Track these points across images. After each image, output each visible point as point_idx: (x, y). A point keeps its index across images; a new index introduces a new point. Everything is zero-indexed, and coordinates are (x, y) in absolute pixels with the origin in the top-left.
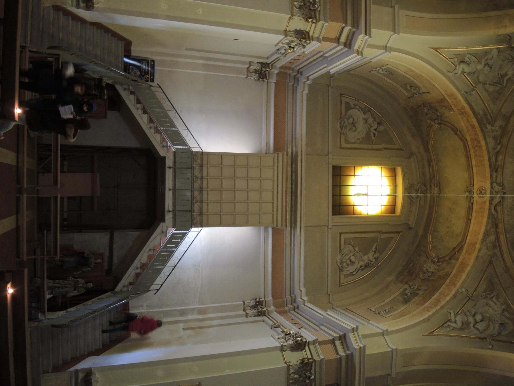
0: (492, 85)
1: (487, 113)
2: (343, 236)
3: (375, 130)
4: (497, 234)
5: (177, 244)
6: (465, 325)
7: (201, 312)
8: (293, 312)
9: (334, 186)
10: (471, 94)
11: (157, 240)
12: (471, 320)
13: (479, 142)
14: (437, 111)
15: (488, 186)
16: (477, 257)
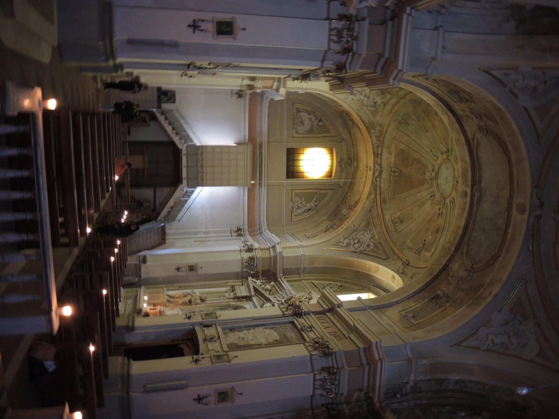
3: (317, 125)
4: (376, 194)
5: (189, 196)
6: (348, 245)
7: (205, 233)
8: (259, 235)
9: (288, 160)
11: (178, 194)
16: (363, 207)
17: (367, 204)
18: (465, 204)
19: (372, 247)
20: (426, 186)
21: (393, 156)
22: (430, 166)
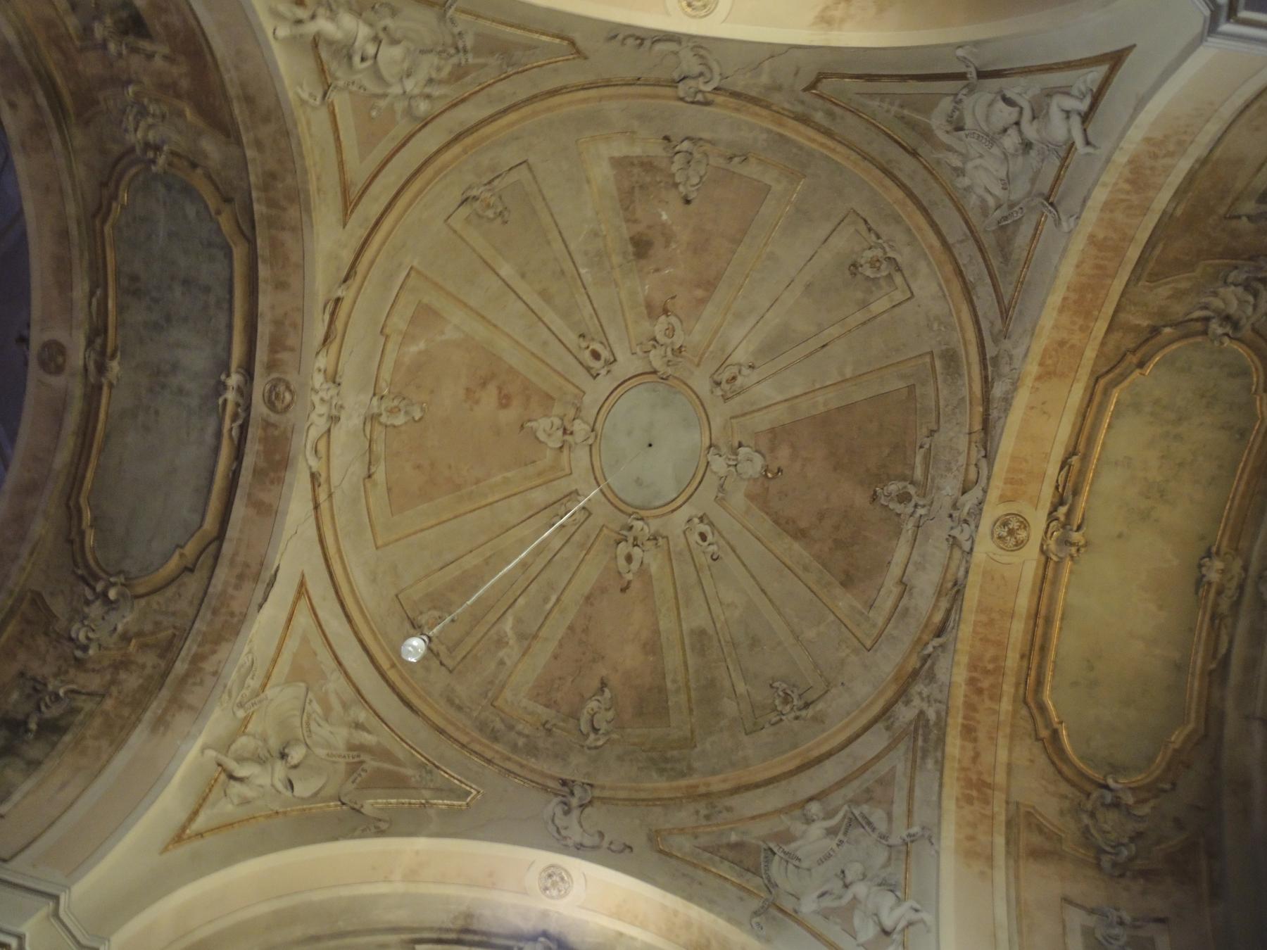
0: (869, 823)
1: (919, 754)
2: (567, 471)
10: (923, 828)
12: (1030, 131)
13: (972, 681)
14: (1086, 831)
15: (985, 548)
17: (1018, 352)
18: (272, 366)
19: (937, 122)
20: (763, 421)
21: (895, 571)
22: (738, 499)
